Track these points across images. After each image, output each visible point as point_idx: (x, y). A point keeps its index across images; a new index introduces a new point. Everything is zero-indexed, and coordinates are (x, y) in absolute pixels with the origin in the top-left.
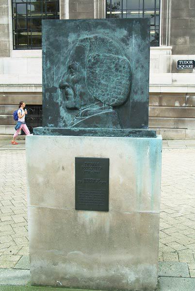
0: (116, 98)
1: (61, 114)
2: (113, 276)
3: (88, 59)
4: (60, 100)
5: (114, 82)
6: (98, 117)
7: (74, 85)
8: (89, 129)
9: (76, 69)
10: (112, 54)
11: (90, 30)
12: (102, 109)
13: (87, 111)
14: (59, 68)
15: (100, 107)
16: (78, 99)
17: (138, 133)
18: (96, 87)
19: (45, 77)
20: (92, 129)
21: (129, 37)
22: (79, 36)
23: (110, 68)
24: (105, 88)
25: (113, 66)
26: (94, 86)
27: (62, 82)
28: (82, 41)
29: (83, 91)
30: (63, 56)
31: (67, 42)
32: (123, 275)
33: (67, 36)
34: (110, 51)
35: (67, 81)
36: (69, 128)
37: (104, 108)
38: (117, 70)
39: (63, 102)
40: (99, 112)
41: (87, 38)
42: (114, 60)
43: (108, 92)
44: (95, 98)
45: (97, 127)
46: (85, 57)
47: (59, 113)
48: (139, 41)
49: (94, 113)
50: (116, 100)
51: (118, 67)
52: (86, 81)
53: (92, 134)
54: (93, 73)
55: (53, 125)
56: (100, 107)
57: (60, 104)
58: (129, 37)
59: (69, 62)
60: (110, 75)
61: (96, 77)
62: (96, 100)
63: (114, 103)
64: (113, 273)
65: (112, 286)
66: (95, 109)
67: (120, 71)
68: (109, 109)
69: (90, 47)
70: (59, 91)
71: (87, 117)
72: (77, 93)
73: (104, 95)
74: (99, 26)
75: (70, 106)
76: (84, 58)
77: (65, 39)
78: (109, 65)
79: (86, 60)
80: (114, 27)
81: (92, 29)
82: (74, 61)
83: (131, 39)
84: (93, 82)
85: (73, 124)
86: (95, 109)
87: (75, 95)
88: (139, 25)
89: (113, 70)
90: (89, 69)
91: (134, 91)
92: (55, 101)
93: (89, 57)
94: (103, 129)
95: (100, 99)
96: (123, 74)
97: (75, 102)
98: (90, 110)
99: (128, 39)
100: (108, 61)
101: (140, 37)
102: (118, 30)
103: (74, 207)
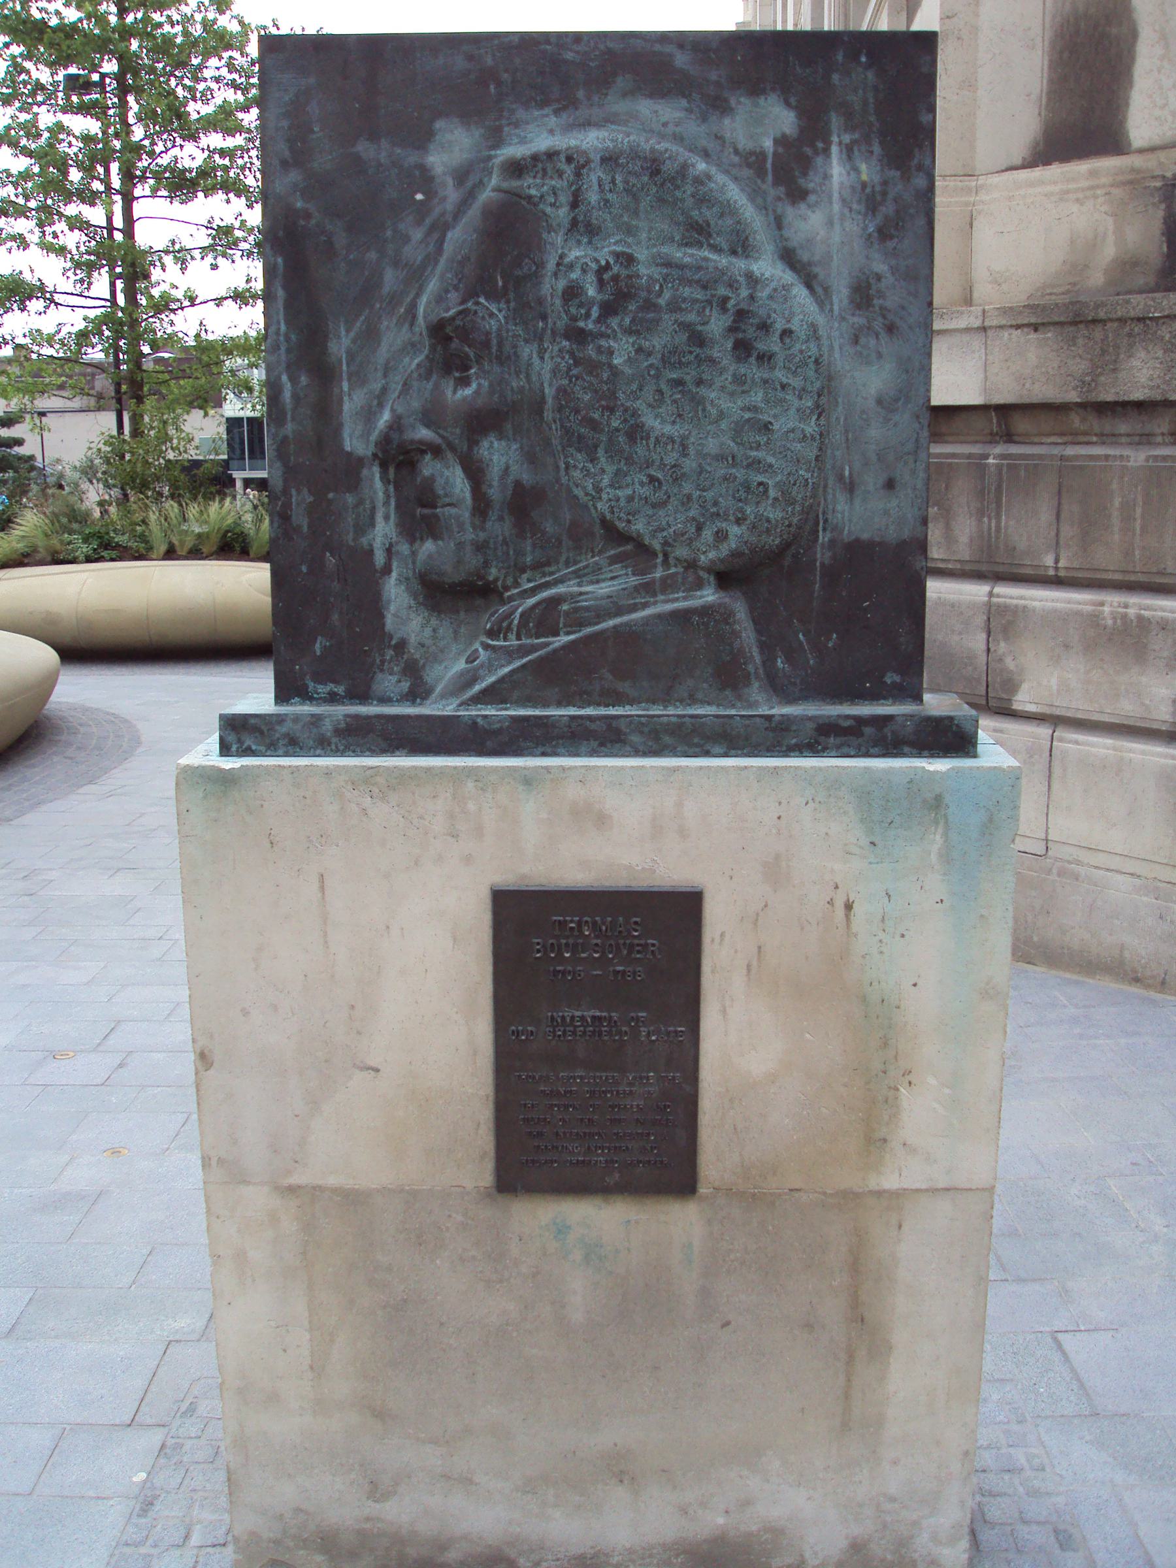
0: (738, 522)
1: (389, 622)
2: (720, 1540)
3: (561, 284)
4: (383, 531)
5: (724, 425)
6: (627, 638)
7: (473, 443)
8: (572, 711)
9: (486, 344)
10: (716, 249)
11: (567, 103)
12: (648, 589)
13: (556, 601)
14: (371, 335)
15: (634, 580)
16: (499, 528)
17: (868, 730)
18: (613, 452)
19: (287, 395)
20: (589, 711)
21: (808, 151)
22: (496, 138)
23: (698, 339)
24: (670, 460)
25: (717, 324)
26: (601, 452)
27: (397, 425)
28: (516, 168)
29: (527, 478)
30: (396, 264)
31: (425, 179)
32: (777, 1532)
33: (422, 138)
34: (698, 233)
35: (429, 417)
36: (447, 708)
37: (667, 585)
38: (743, 349)
39: (404, 548)
40: (634, 608)
41: (551, 155)
42: (722, 291)
43: (687, 487)
44: (604, 522)
45: (618, 699)
46: (541, 265)
47: (373, 606)
48: (867, 171)
49: (600, 614)
50: (734, 530)
51: (751, 333)
52: (548, 415)
53: (594, 744)
54: (593, 367)
55: (340, 690)
56: (634, 580)
57: (380, 558)
58: (808, 151)
59: (440, 299)
60: (699, 382)
61: (613, 395)
62: (614, 534)
63: (725, 550)
64: (721, 1520)
65: (762, 101)
66: (604, 589)
67: (765, 358)
68: (699, 585)
69: (574, 205)
70: (375, 483)
71: (564, 639)
72: (495, 492)
73: (663, 504)
74: (622, 82)
75: (453, 575)
76: (535, 277)
77: (412, 158)
78: (692, 317)
79: (551, 287)
80: (718, 84)
81: (200, 497)
82: (471, 294)
83: (819, 160)
84: (594, 425)
85: (474, 680)
86: (604, 589)
87: (481, 505)
88: (870, 75)
89: (722, 350)
90: (565, 343)
91: (841, 478)
92: (349, 538)
93: (571, 266)
94: (656, 711)
95: (639, 526)
96: (780, 375)
97: (480, 547)
98: (572, 597)
99: (806, 164)
100: (687, 291)
101: (877, 149)
102: (743, 104)
103: (486, 1176)
